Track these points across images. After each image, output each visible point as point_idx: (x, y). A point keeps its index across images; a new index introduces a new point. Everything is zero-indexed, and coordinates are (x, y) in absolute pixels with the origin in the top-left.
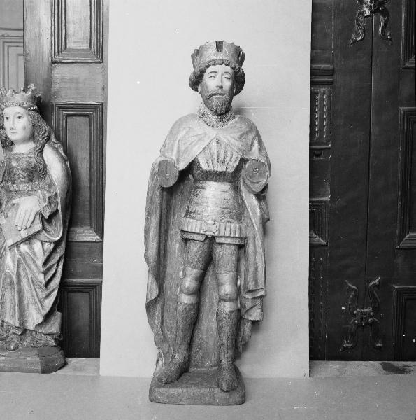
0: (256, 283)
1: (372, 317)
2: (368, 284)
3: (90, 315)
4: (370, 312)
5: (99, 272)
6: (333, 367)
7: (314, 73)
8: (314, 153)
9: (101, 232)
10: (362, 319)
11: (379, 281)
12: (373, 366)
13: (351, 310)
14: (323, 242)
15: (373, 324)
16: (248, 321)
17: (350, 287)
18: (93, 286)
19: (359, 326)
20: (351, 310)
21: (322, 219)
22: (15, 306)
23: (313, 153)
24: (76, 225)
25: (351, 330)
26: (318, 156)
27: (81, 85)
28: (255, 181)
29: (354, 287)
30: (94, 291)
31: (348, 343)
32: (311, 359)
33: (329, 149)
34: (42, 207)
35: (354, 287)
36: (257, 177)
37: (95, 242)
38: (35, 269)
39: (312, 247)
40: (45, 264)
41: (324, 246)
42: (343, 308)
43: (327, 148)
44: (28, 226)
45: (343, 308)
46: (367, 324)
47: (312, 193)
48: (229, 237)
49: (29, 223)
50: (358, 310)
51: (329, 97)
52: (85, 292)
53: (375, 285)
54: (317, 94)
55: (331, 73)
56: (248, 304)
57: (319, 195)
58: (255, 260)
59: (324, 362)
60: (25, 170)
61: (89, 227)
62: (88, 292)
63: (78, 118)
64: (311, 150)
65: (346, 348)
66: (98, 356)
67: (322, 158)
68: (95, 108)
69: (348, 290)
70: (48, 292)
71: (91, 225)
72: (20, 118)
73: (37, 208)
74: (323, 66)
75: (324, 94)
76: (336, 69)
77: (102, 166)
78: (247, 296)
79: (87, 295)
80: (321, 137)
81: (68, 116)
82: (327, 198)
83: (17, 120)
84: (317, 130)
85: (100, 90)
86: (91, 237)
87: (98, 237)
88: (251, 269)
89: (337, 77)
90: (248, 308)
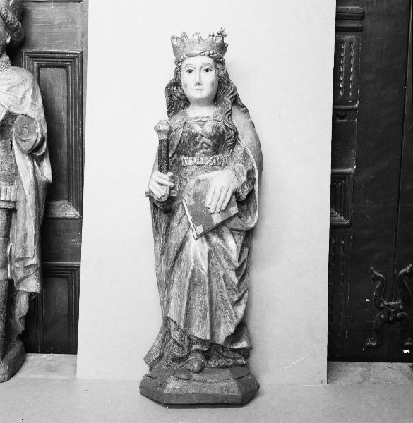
0: (25, 250)
1: (401, 311)
2: (398, 273)
3: (69, 301)
4: (399, 304)
5: (77, 254)
6: (355, 370)
7: (340, 17)
8: (338, 115)
9: (79, 206)
10: (389, 313)
11: (411, 269)
12: (402, 369)
13: (376, 303)
14: (346, 222)
15: (401, 319)
16: (24, 293)
17: (375, 275)
18: (72, 270)
19: (386, 321)
20: (376, 303)
21: (345, 195)
22: (205, 313)
23: (337, 114)
24: (57, 199)
25: (376, 325)
26: (342, 118)
27: (56, 30)
28: (24, 139)
29: (382, 276)
30: (73, 275)
31: (372, 341)
32: (330, 359)
33: (356, 109)
34: (240, 184)
35: (382, 276)
36: (26, 133)
37: (74, 219)
38: (226, 265)
39: (334, 228)
40: (239, 260)
41: (347, 226)
42: (367, 300)
43: (352, 109)
44: (223, 209)
45: (367, 300)
46: (395, 319)
47: (335, 162)
48: (5, 201)
49: (225, 204)
50: (385, 302)
51: (357, 47)
52: (63, 277)
53: (406, 272)
54: (343, 42)
55: (361, 17)
56: (20, 274)
57: (341, 166)
58: (24, 225)
59: (344, 364)
60: (212, 138)
61: (66, 201)
62: (67, 278)
63: (53, 70)
64: (334, 110)
65: (370, 347)
66: (75, 352)
67: (346, 120)
68: (73, 58)
69: (374, 279)
70: (240, 294)
71: (69, 199)
72: (207, 70)
73: (234, 185)
74: (350, 8)
75: (351, 43)
76: (366, 13)
77: (82, 128)
78: (17, 265)
79: (65, 281)
80: (346, 94)
81: (40, 67)
82: (351, 170)
83: (204, 73)
84: (341, 86)
85: (79, 36)
86: (71, 213)
87: (78, 213)
88: (20, 235)
89: (368, 24)
90: (19, 278)
